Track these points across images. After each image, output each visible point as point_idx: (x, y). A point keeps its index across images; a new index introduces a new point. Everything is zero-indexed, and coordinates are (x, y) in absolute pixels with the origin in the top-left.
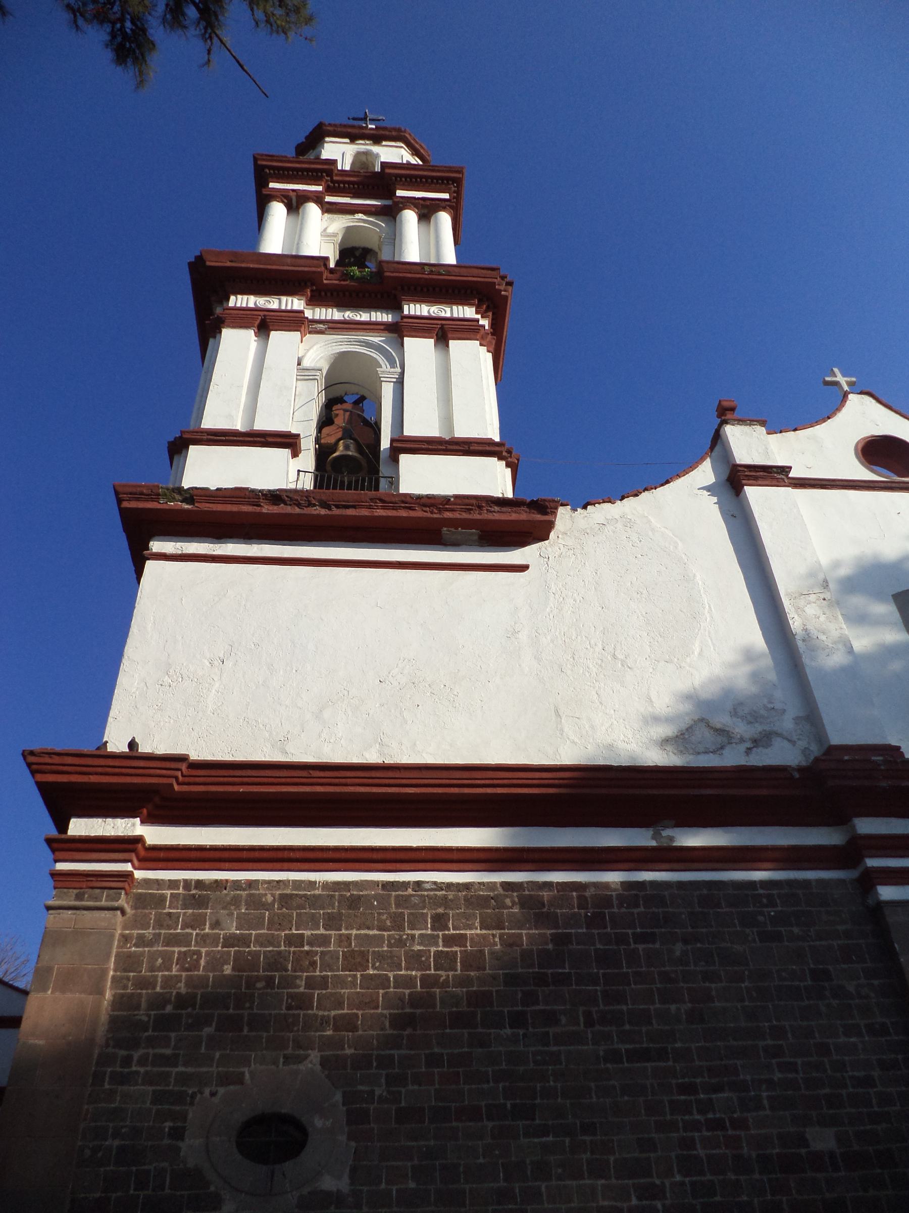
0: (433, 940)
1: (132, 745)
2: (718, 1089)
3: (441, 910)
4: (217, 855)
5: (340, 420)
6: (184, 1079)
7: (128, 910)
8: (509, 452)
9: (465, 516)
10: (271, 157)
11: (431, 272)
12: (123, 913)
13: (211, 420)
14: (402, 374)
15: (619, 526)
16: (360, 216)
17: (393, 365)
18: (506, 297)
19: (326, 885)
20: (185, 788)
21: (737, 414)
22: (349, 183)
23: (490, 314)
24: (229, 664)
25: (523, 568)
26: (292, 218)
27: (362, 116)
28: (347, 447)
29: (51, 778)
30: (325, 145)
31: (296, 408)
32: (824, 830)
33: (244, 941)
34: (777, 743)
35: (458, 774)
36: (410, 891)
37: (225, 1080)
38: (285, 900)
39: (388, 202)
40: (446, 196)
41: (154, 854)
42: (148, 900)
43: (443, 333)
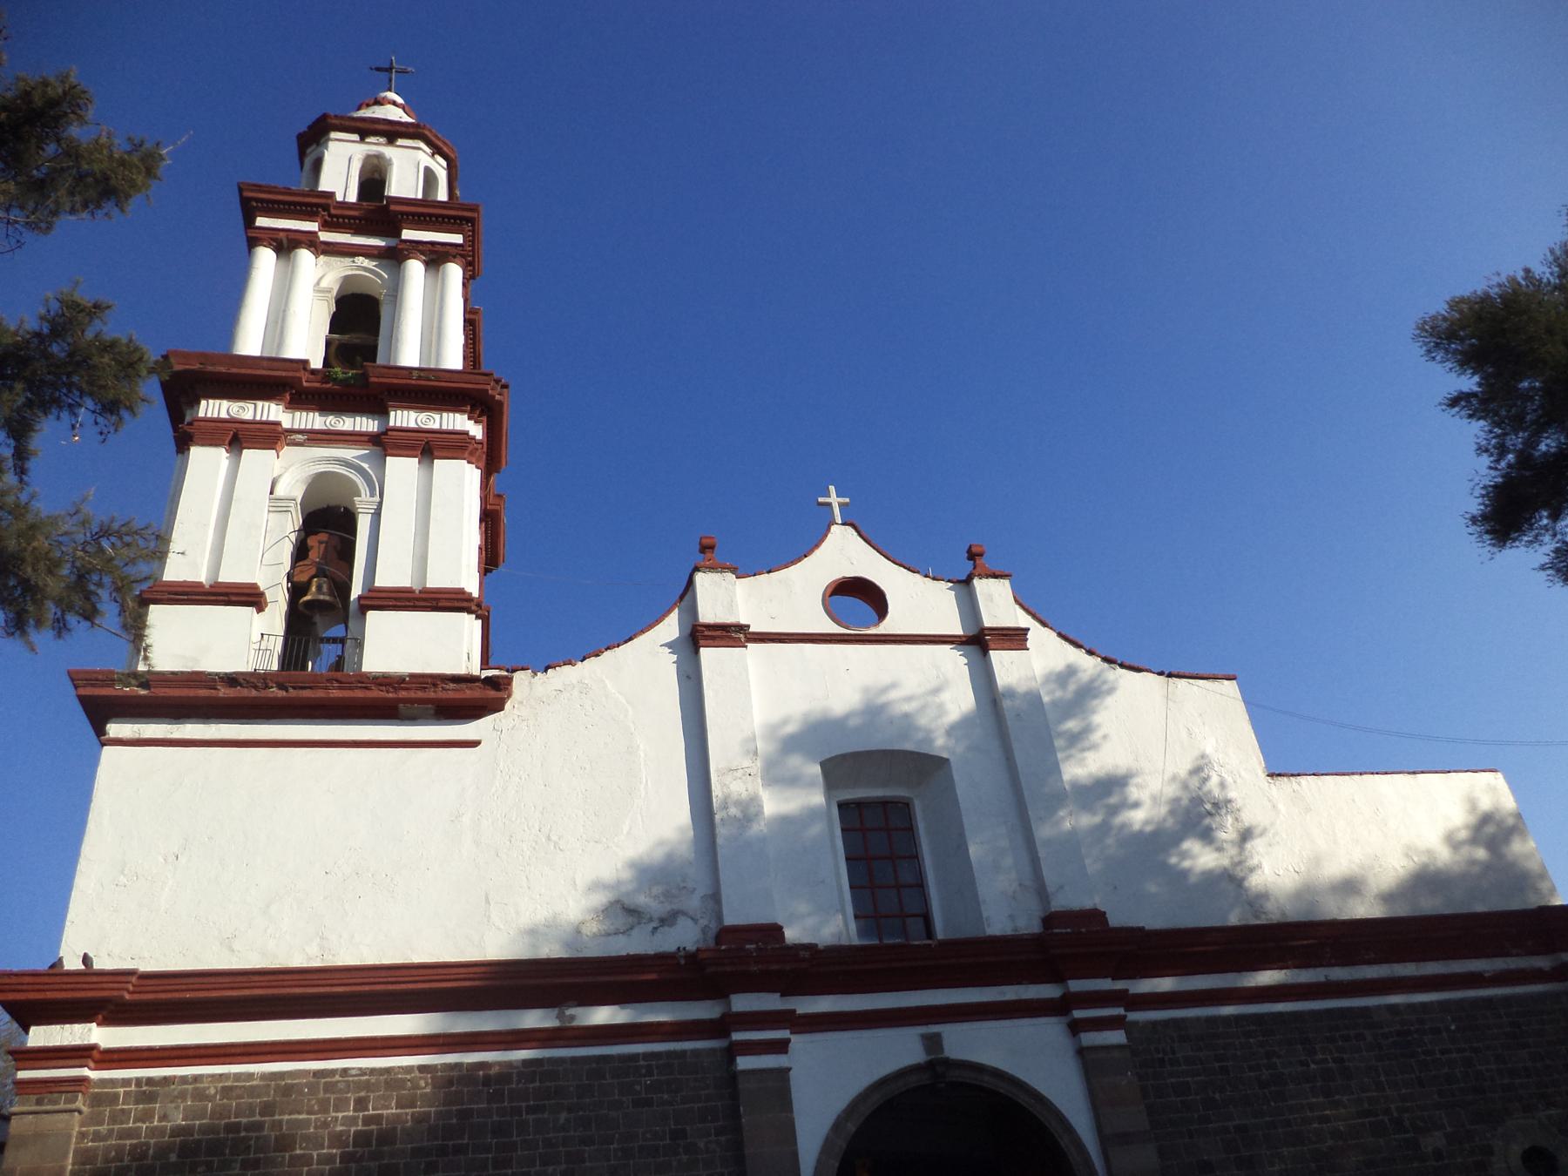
0: (354, 1120)
1: (86, 959)
3: (363, 1094)
4: (166, 1054)
5: (314, 555)
7: (85, 1109)
8: (479, 606)
9: (420, 694)
10: (259, 188)
11: (419, 378)
12: (80, 1112)
13: (175, 571)
14: (380, 504)
15: (576, 693)
16: (360, 260)
17: (372, 495)
18: (500, 404)
19: (264, 1076)
20: (137, 997)
21: (717, 555)
22: (349, 217)
23: (484, 419)
24: (183, 860)
25: (474, 744)
26: (282, 262)
28: (319, 588)
29: (11, 996)
30: (331, 144)
31: (264, 552)
32: (708, 1003)
34: (682, 922)
35: (383, 973)
36: (337, 1078)
38: (226, 1091)
39: (392, 242)
40: (457, 239)
41: (107, 1057)
42: (103, 1098)
43: (429, 447)
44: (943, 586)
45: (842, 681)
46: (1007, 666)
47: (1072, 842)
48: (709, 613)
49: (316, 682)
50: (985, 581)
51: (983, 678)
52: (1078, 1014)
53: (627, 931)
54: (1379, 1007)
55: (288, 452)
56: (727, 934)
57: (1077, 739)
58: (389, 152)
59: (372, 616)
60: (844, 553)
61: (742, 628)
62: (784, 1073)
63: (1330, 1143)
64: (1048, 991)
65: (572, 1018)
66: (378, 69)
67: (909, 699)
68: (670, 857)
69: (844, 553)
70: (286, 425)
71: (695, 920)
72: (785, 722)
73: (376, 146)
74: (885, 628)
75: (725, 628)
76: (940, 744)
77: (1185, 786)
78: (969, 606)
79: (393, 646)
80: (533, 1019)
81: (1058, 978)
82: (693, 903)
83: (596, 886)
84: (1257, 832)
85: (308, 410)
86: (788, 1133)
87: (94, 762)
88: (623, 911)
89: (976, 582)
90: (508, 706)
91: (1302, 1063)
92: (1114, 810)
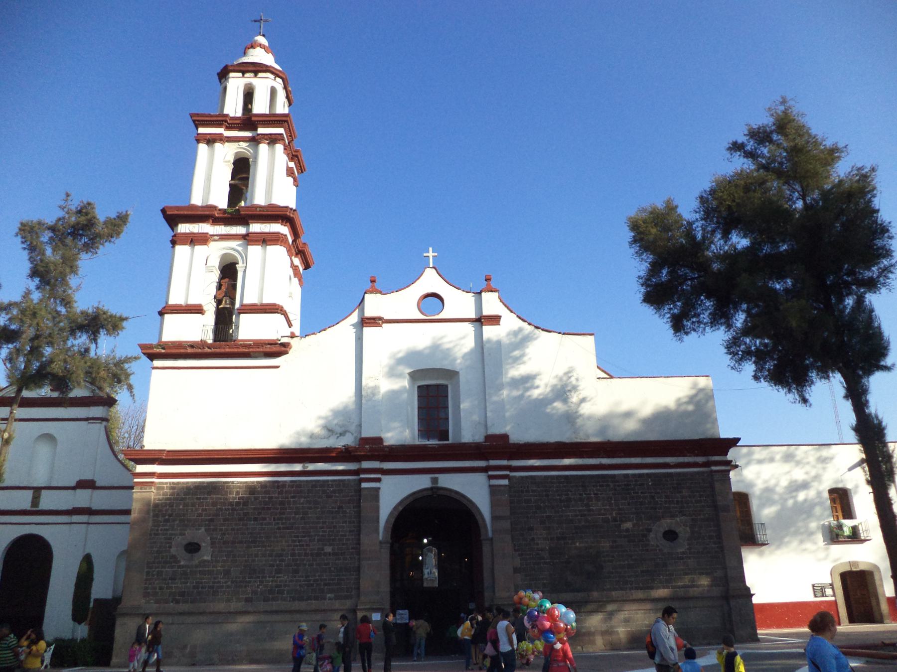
5: (224, 288)
6: (171, 534)
10: (198, 115)
16: (241, 143)
25: (277, 367)
30: (230, 80)
32: (355, 464)
34: (348, 434)
37: (181, 534)
43: (266, 240)
47: (501, 405)
48: (368, 313)
51: (479, 335)
52: (490, 473)
56: (364, 441)
57: (517, 360)
60: (430, 281)
61: (380, 318)
62: (379, 488)
67: (450, 342)
68: (346, 407)
69: (430, 281)
70: (211, 233)
72: (399, 352)
73: (249, 79)
74: (441, 316)
75: (374, 319)
76: (458, 364)
77: (561, 379)
78: (479, 305)
79: (249, 328)
80: (298, 467)
81: (487, 459)
82: (353, 428)
83: (320, 418)
88: (330, 430)
89: (483, 294)
92: (528, 389)
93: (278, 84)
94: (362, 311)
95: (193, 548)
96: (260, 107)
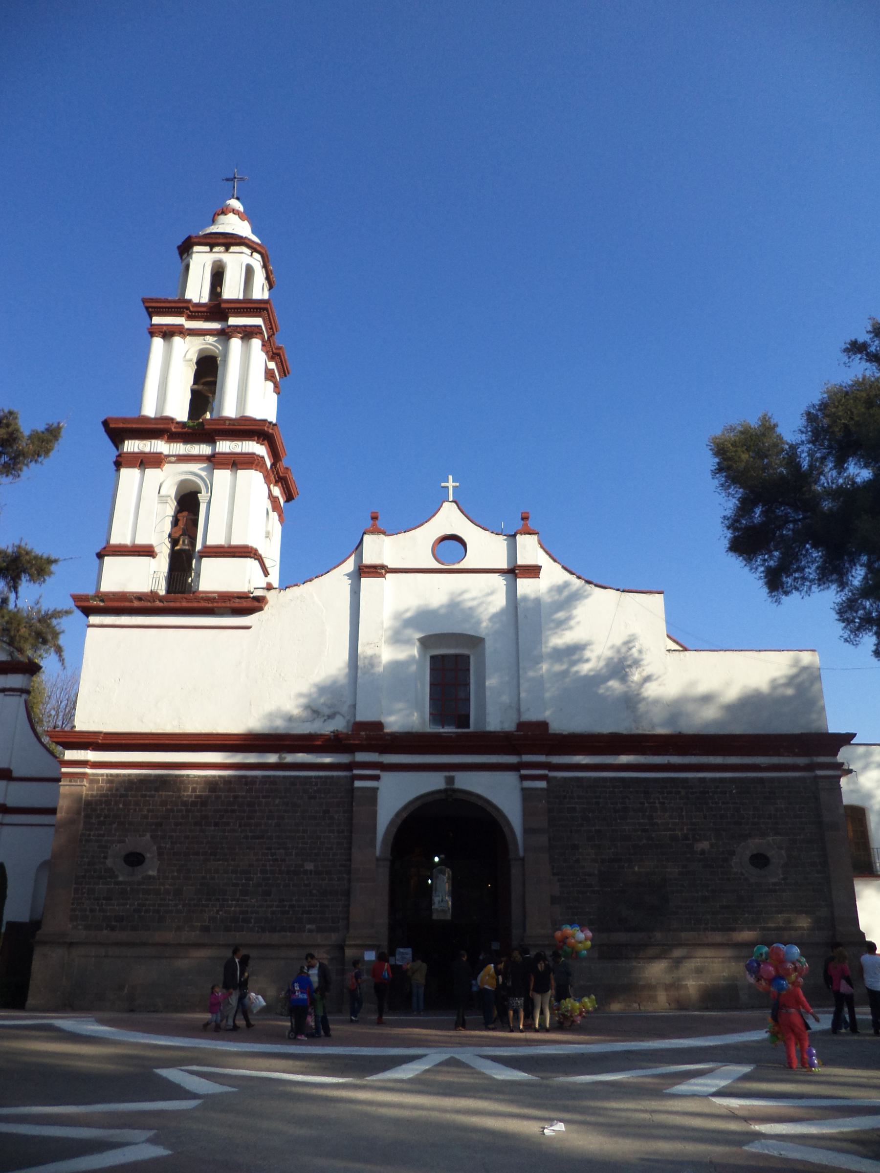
2: (278, 849)
5: (181, 524)
11: (229, 425)
22: (201, 312)
27: (232, 177)
28: (184, 542)
30: (194, 256)
31: (156, 528)
33: (126, 796)
34: (339, 718)
37: (120, 842)
39: (225, 326)
44: (502, 538)
45: (437, 591)
46: (525, 586)
48: (369, 559)
49: (180, 597)
50: (523, 536)
51: (512, 590)
52: (523, 772)
53: (312, 721)
54: (693, 778)
55: (167, 467)
57: (561, 624)
58: (226, 258)
59: (205, 561)
60: (449, 519)
61: (383, 567)
62: (375, 790)
63: (645, 841)
64: (512, 759)
65: (285, 758)
66: (227, 180)
67: (473, 599)
69: (449, 519)
70: (166, 452)
71: (343, 716)
72: (407, 611)
73: (219, 254)
76: (484, 627)
77: (618, 651)
79: (214, 577)
81: (518, 753)
82: (345, 709)
84: (655, 677)
85: (177, 442)
86: (374, 815)
87: (83, 636)
88: (313, 711)
89: (518, 537)
90: (266, 608)
91: (641, 803)
92: (575, 663)
93: (256, 262)
94: (360, 557)
95: (135, 859)
96: (232, 290)
